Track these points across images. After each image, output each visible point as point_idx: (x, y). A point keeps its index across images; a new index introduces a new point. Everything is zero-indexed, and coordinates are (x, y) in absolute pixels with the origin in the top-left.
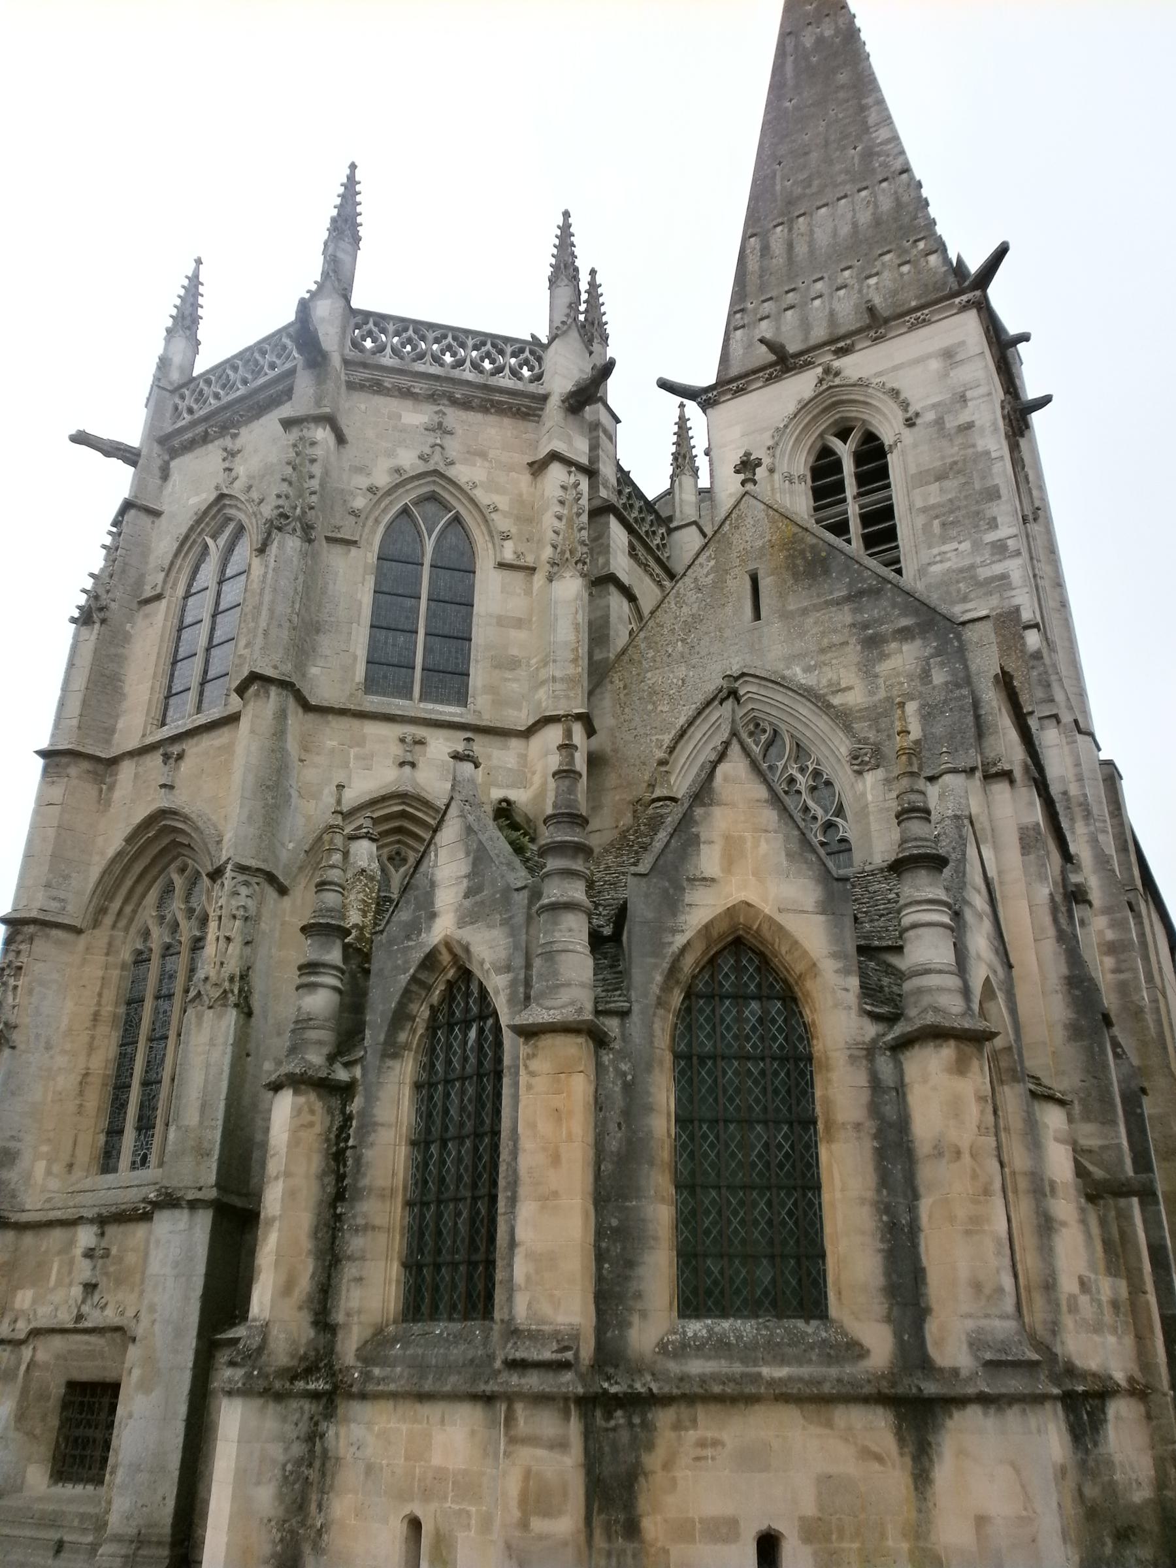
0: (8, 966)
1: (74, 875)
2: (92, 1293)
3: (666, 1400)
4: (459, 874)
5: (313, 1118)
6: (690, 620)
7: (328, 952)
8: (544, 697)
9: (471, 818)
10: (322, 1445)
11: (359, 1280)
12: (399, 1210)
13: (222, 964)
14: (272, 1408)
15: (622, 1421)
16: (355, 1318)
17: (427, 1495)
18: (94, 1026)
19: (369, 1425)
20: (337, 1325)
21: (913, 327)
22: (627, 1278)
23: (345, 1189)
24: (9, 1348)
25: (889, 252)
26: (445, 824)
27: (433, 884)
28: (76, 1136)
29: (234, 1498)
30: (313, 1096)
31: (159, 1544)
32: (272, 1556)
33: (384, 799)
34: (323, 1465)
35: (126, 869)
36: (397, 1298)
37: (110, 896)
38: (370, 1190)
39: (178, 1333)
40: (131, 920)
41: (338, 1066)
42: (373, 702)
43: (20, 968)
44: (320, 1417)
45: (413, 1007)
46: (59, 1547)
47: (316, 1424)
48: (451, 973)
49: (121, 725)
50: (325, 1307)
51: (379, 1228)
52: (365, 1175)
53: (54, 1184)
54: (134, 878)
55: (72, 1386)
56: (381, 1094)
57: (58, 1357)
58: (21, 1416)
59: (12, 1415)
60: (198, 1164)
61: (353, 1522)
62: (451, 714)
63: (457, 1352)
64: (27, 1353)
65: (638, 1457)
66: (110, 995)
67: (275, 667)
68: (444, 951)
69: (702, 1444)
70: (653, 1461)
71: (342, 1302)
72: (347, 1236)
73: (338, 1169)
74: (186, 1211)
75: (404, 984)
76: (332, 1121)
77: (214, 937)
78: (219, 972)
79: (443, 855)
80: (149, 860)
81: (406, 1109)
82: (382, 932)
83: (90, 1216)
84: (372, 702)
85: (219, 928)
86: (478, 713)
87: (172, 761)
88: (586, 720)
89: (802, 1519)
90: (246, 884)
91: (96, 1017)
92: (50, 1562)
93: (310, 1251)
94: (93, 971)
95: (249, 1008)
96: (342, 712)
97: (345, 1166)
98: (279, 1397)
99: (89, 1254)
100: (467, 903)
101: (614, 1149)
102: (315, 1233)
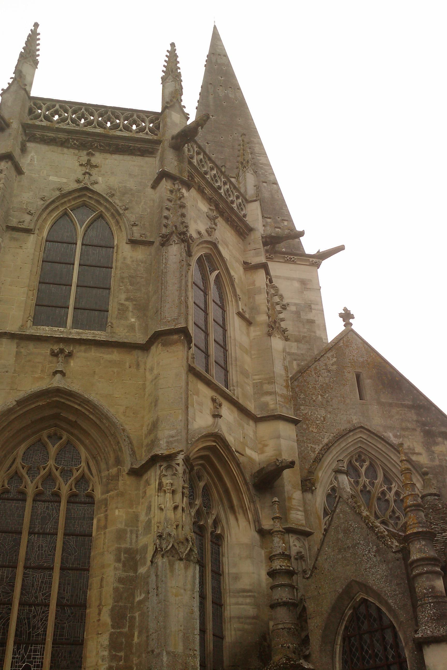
6: (324, 385)
21: (287, 262)
25: (270, 218)
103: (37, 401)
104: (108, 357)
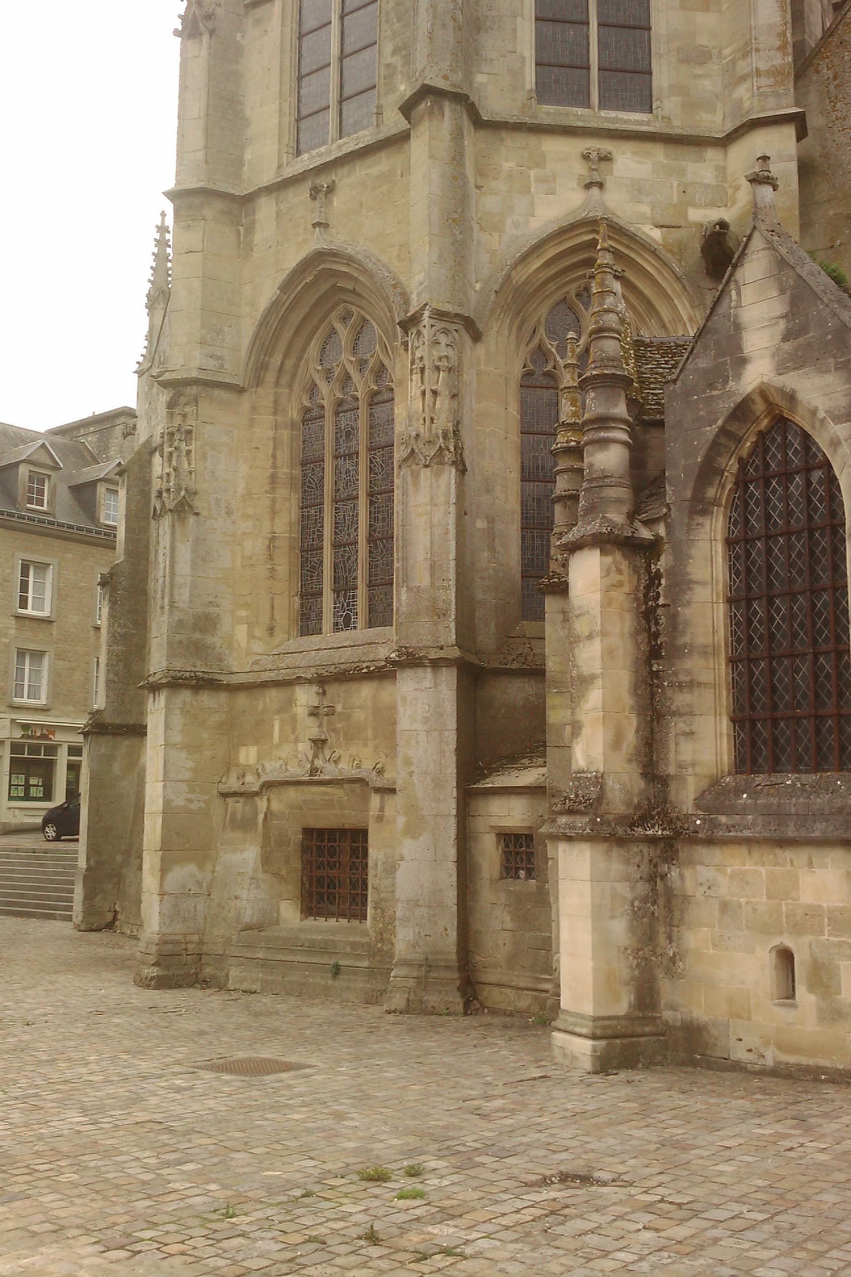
0: (178, 430)
1: (226, 329)
2: (322, 748)
4: (773, 315)
5: (621, 578)
7: (616, 405)
8: (746, 97)
9: (783, 251)
10: (666, 886)
11: (690, 734)
12: (724, 667)
13: (432, 419)
14: (616, 852)
16: (690, 770)
17: (798, 929)
18: (274, 489)
19: (720, 868)
20: (668, 776)
23: (660, 647)
24: (241, 800)
26: (747, 259)
27: (738, 327)
28: (272, 598)
29: (594, 929)
30: (618, 556)
31: (447, 968)
32: (632, 979)
33: (573, 227)
34: (669, 901)
35: (284, 320)
36: (729, 750)
37: (270, 351)
38: (692, 648)
39: (438, 784)
40: (294, 376)
41: (637, 524)
42: (549, 113)
43: (189, 432)
44: (658, 860)
45: (722, 461)
46: (337, 971)
47: (655, 866)
48: (764, 423)
49: (248, 156)
50: (651, 760)
51: (705, 684)
52: (683, 633)
53: (258, 647)
54: (294, 329)
55: (308, 832)
56: (694, 552)
57: (292, 807)
58: (266, 860)
59: (259, 859)
60: (435, 624)
61: (711, 951)
63: (820, 801)
64: (262, 804)
66: (284, 456)
67: (446, 77)
68: (758, 400)
71: (672, 755)
72: (669, 693)
73: (650, 628)
74: (429, 670)
75: (711, 437)
76: (639, 579)
77: (419, 392)
78: (430, 430)
79: (748, 295)
80: (307, 310)
81: (721, 564)
82: (675, 381)
83: (309, 676)
84: (548, 113)
85: (422, 383)
86: (667, 119)
87: (321, 195)
88: (799, 122)
90: (446, 332)
91: (273, 479)
92: (330, 982)
93: (632, 706)
94: (264, 432)
95: (464, 465)
96: (518, 127)
97: (657, 624)
98: (621, 842)
99: (314, 713)
100: (787, 346)
102: (635, 690)
103: (304, 278)
104: (375, 170)
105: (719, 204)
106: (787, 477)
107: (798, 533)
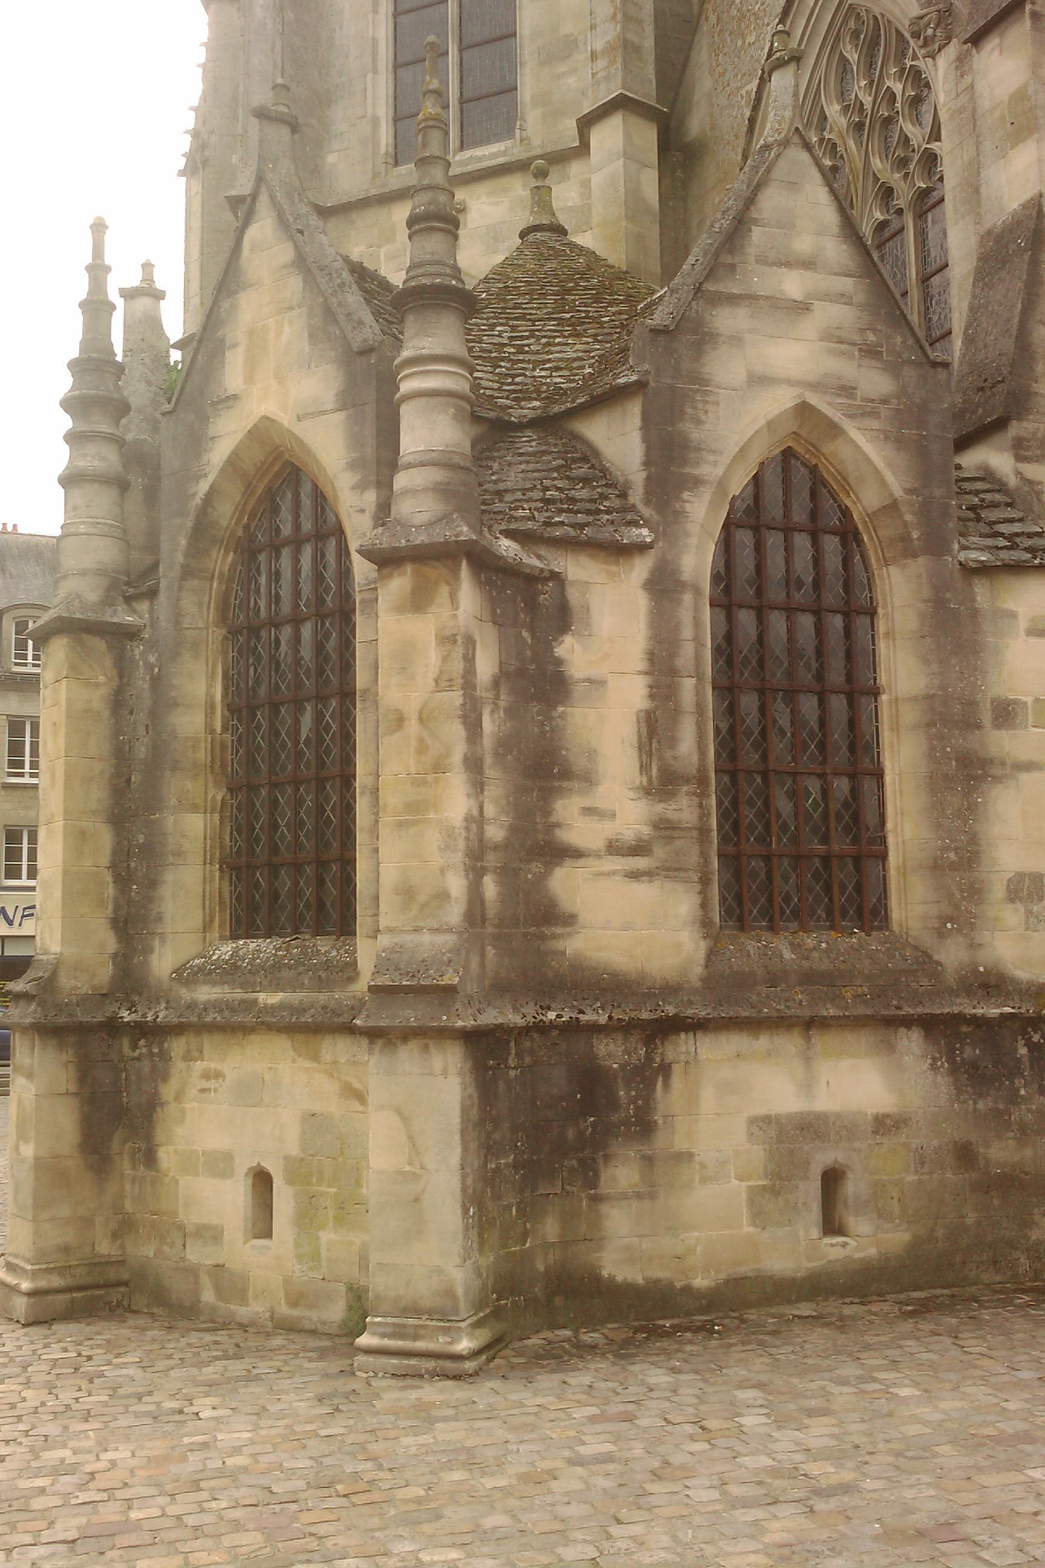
3: (179, 1029)
15: (144, 1050)
22: (150, 900)
62: (494, 156)
65: (156, 1088)
69: (206, 1075)
70: (168, 1091)
89: (286, 1158)
101: (142, 756)
105: (585, 228)
106: (297, 543)
107: (332, 614)
